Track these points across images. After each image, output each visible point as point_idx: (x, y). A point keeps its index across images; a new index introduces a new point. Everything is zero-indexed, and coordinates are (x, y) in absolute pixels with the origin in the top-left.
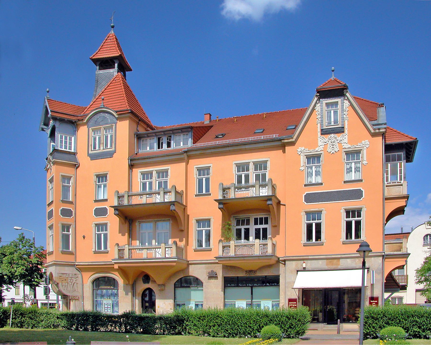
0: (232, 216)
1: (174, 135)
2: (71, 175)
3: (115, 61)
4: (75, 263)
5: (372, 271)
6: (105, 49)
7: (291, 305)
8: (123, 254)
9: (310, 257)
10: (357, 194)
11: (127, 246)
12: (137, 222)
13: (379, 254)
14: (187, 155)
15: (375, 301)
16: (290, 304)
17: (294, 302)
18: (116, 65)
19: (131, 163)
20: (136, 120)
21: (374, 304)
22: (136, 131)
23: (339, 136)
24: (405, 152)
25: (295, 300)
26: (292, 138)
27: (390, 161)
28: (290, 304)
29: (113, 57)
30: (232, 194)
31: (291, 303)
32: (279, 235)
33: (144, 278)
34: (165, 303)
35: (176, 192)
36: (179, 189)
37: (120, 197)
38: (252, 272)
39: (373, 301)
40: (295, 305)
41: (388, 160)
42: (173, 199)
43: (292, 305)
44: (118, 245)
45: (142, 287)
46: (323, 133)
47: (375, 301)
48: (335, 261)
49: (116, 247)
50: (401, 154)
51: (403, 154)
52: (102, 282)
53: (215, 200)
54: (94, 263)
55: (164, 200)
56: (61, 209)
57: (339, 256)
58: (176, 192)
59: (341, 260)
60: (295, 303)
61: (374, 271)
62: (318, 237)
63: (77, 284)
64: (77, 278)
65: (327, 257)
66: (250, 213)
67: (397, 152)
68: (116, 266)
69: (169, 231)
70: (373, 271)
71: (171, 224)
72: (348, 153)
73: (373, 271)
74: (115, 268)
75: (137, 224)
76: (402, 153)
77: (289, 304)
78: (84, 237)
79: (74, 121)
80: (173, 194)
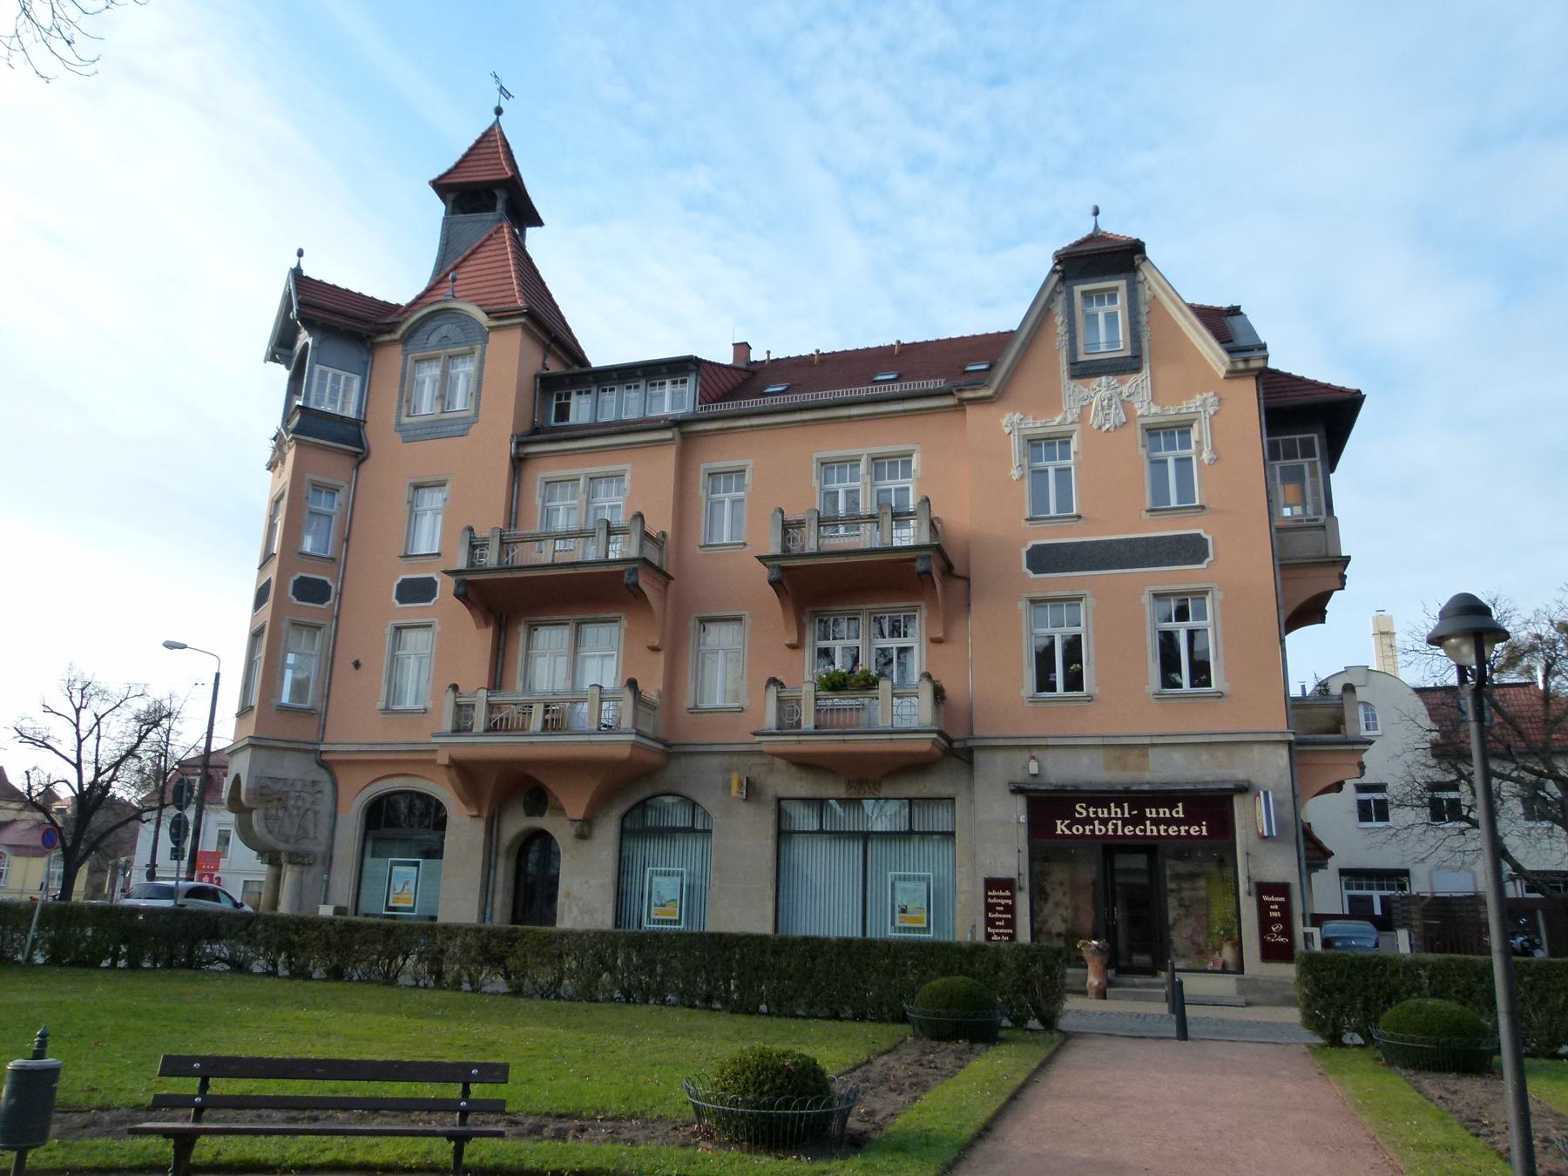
0: (808, 609)
1: (647, 381)
2: (342, 483)
3: (497, 192)
4: (317, 747)
5: (1262, 793)
6: (472, 164)
7: (995, 901)
8: (468, 717)
9: (1050, 742)
10: (1191, 549)
11: (483, 693)
12: (523, 622)
13: (1278, 737)
14: (682, 433)
15: (1277, 899)
16: (992, 897)
17: (1004, 891)
18: (500, 206)
19: (517, 453)
20: (544, 339)
21: (1276, 907)
22: (539, 367)
23: (1122, 383)
24: (1323, 433)
25: (1007, 884)
26: (987, 386)
27: (1279, 459)
28: (992, 897)
29: (493, 181)
30: (810, 541)
31: (994, 893)
32: (1323, 621)
33: (528, 799)
34: (587, 882)
35: (646, 535)
36: (654, 527)
37: (474, 546)
38: (866, 787)
39: (1273, 899)
40: (1007, 901)
41: (1273, 453)
42: (633, 553)
43: (999, 901)
44: (455, 687)
45: (516, 824)
46: (1075, 373)
47: (1277, 899)
48: (1133, 756)
49: (451, 694)
50: (1313, 438)
51: (1319, 438)
52: (409, 799)
53: (759, 558)
54: (378, 748)
55: (607, 556)
56: (296, 577)
57: (1147, 741)
58: (646, 535)
59: (1152, 752)
60: (1008, 893)
61: (1270, 793)
62: (1074, 682)
63: (316, 813)
64: (318, 796)
65: (1106, 741)
66: (862, 603)
67: (1280, 435)
68: (443, 758)
69: (615, 653)
70: (1266, 794)
71: (623, 631)
72: (1152, 431)
73: (1266, 794)
74: (439, 762)
75: (522, 630)
76: (1316, 436)
77: (987, 897)
78: (357, 665)
79: (364, 336)
80: (635, 539)
